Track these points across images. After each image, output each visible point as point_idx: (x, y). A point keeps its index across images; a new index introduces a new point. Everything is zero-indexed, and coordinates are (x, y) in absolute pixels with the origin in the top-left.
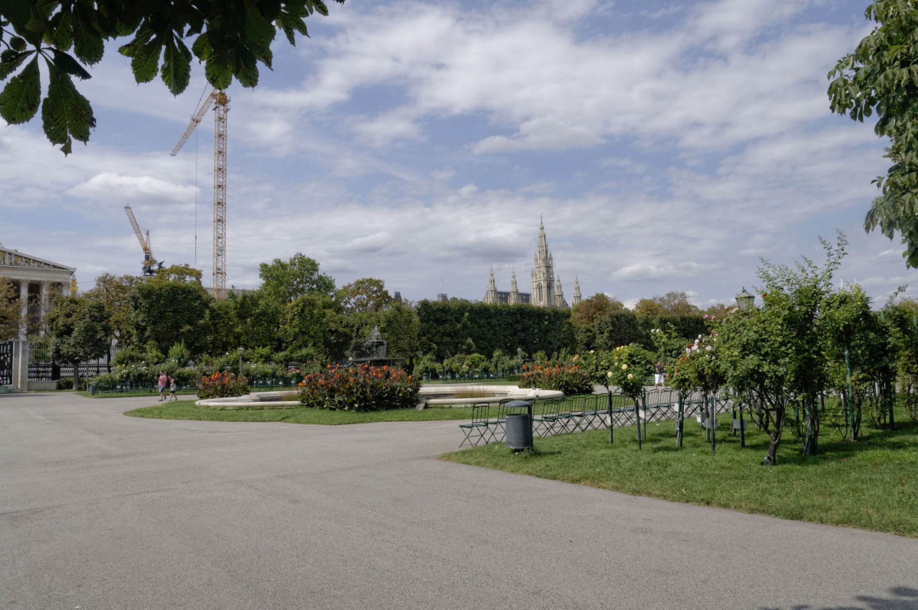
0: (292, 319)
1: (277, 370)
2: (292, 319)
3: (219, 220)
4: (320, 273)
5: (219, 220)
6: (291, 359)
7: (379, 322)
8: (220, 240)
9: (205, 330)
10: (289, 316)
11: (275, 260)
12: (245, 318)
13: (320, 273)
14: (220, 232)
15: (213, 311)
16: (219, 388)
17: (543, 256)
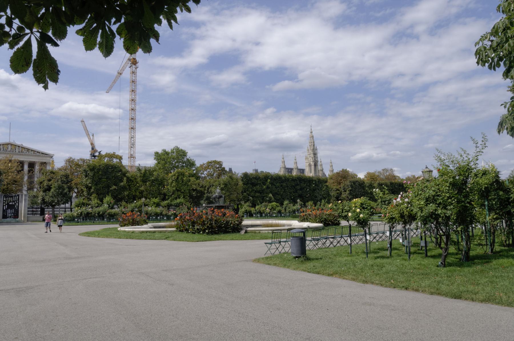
0: (172, 183)
1: (163, 211)
2: (172, 183)
3: (132, 128)
4: (188, 157)
5: (132, 128)
6: (171, 205)
7: (220, 184)
8: (133, 139)
9: (124, 188)
10: (170, 181)
11: (163, 150)
12: (146, 182)
13: (188, 157)
14: (133, 134)
15: (128, 178)
16: (131, 221)
17: (312, 148)
